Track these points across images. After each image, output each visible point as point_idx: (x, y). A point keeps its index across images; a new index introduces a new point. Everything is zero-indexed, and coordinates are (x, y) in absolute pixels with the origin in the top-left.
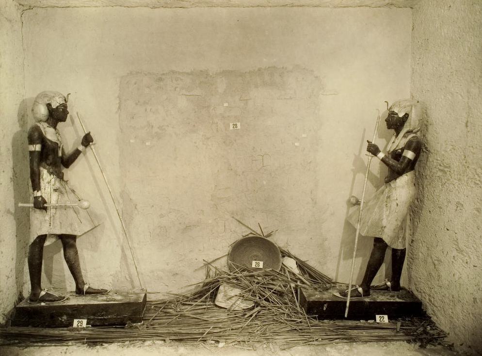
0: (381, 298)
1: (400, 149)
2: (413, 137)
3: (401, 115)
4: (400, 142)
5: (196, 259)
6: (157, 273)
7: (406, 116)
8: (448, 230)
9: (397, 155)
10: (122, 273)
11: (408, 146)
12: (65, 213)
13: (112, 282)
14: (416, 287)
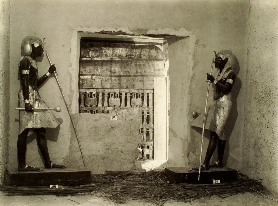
0: (215, 170)
1: (224, 79)
2: (231, 71)
3: (224, 59)
4: (224, 74)
5: (117, 149)
6: (92, 157)
7: (227, 59)
8: (268, 127)
9: (223, 82)
10: (70, 157)
11: (229, 77)
12: (43, 114)
13: (63, 163)
14: (247, 165)
